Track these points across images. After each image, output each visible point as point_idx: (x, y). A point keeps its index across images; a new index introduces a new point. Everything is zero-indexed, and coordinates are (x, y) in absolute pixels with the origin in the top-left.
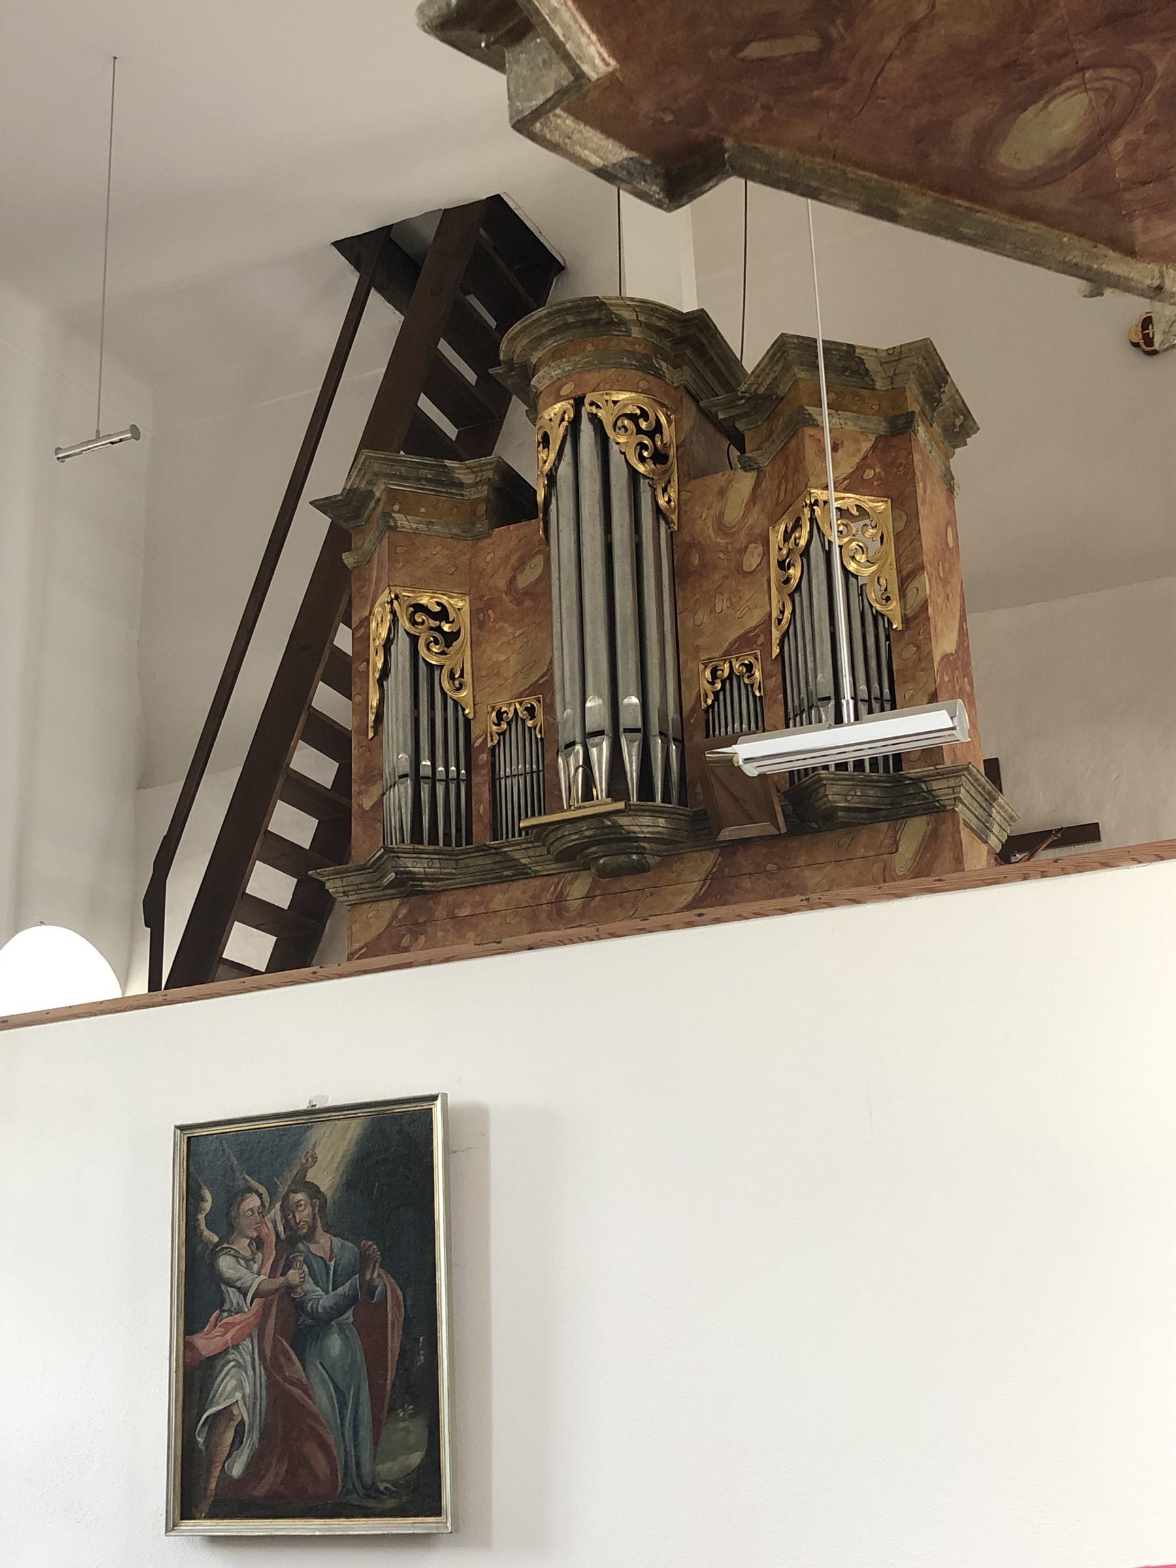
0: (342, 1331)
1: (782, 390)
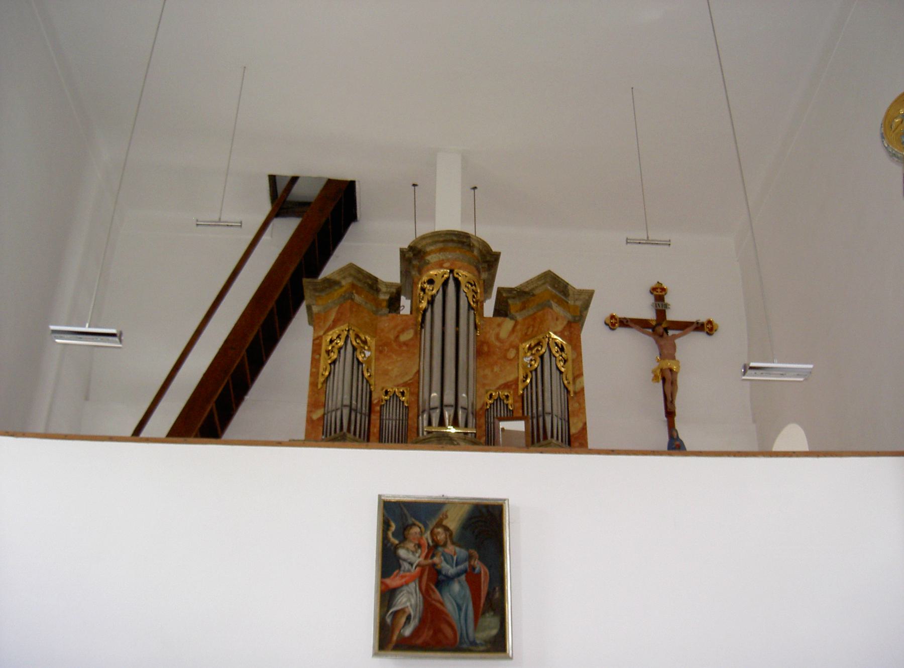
0: (459, 582)
1: (537, 292)
